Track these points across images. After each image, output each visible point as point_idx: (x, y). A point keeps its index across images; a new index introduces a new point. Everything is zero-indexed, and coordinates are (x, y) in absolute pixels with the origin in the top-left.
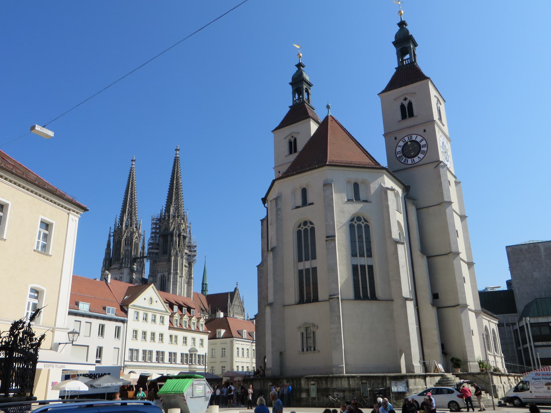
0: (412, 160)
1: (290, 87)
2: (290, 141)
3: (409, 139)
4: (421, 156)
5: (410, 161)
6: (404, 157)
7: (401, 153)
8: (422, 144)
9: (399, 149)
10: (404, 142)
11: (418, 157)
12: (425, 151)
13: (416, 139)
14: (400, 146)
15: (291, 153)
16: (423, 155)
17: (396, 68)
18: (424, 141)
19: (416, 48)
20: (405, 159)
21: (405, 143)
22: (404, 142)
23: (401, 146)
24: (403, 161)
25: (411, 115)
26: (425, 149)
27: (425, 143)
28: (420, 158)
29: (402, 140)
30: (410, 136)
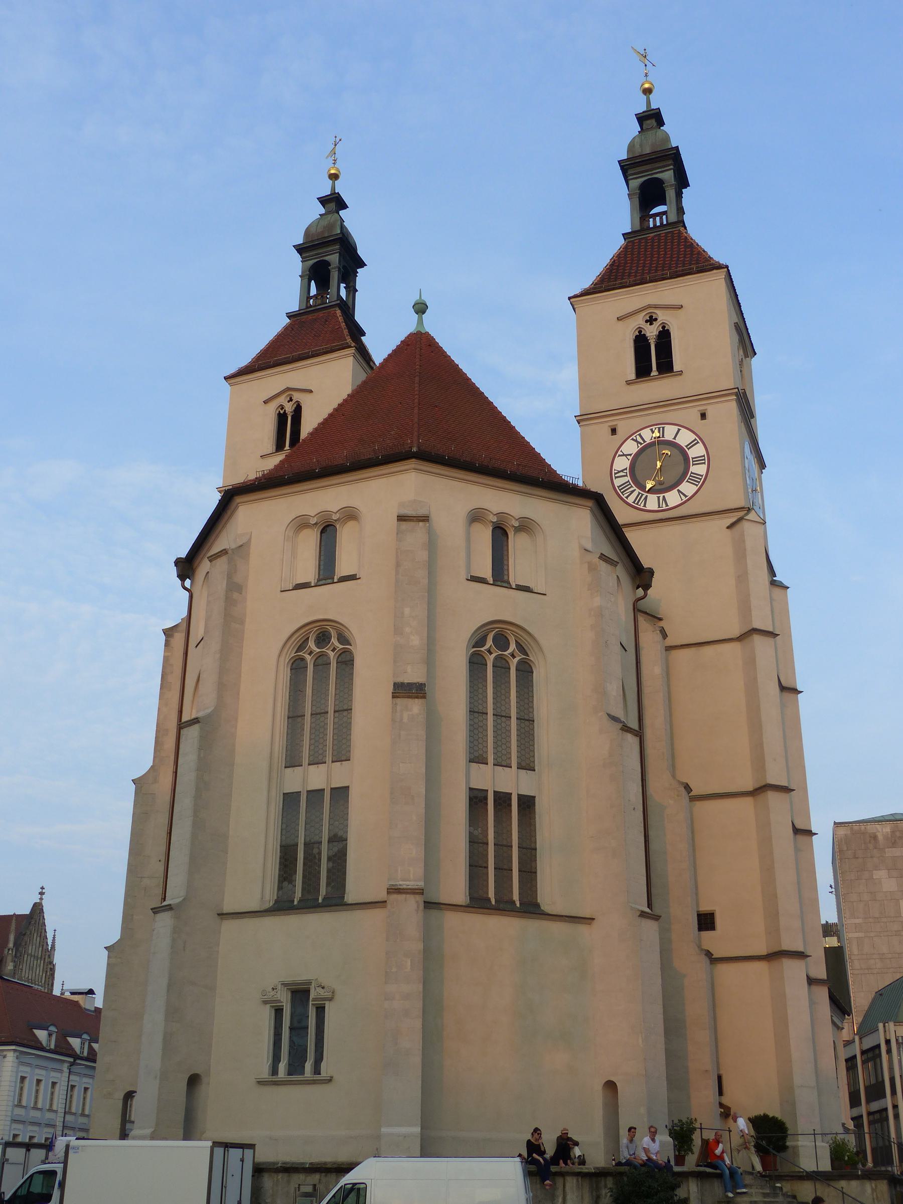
0: (659, 498)
1: (297, 257)
2: (282, 412)
4: (688, 488)
5: (652, 502)
7: (626, 476)
8: (692, 453)
9: (622, 463)
10: (638, 442)
11: (679, 491)
12: (695, 439)
13: (675, 438)
14: (626, 455)
16: (695, 488)
17: (290, 316)
21: (640, 446)
22: (638, 442)
23: (630, 455)
24: (631, 500)
25: (666, 367)
26: (701, 469)
27: (704, 452)
29: (633, 437)
30: (659, 428)
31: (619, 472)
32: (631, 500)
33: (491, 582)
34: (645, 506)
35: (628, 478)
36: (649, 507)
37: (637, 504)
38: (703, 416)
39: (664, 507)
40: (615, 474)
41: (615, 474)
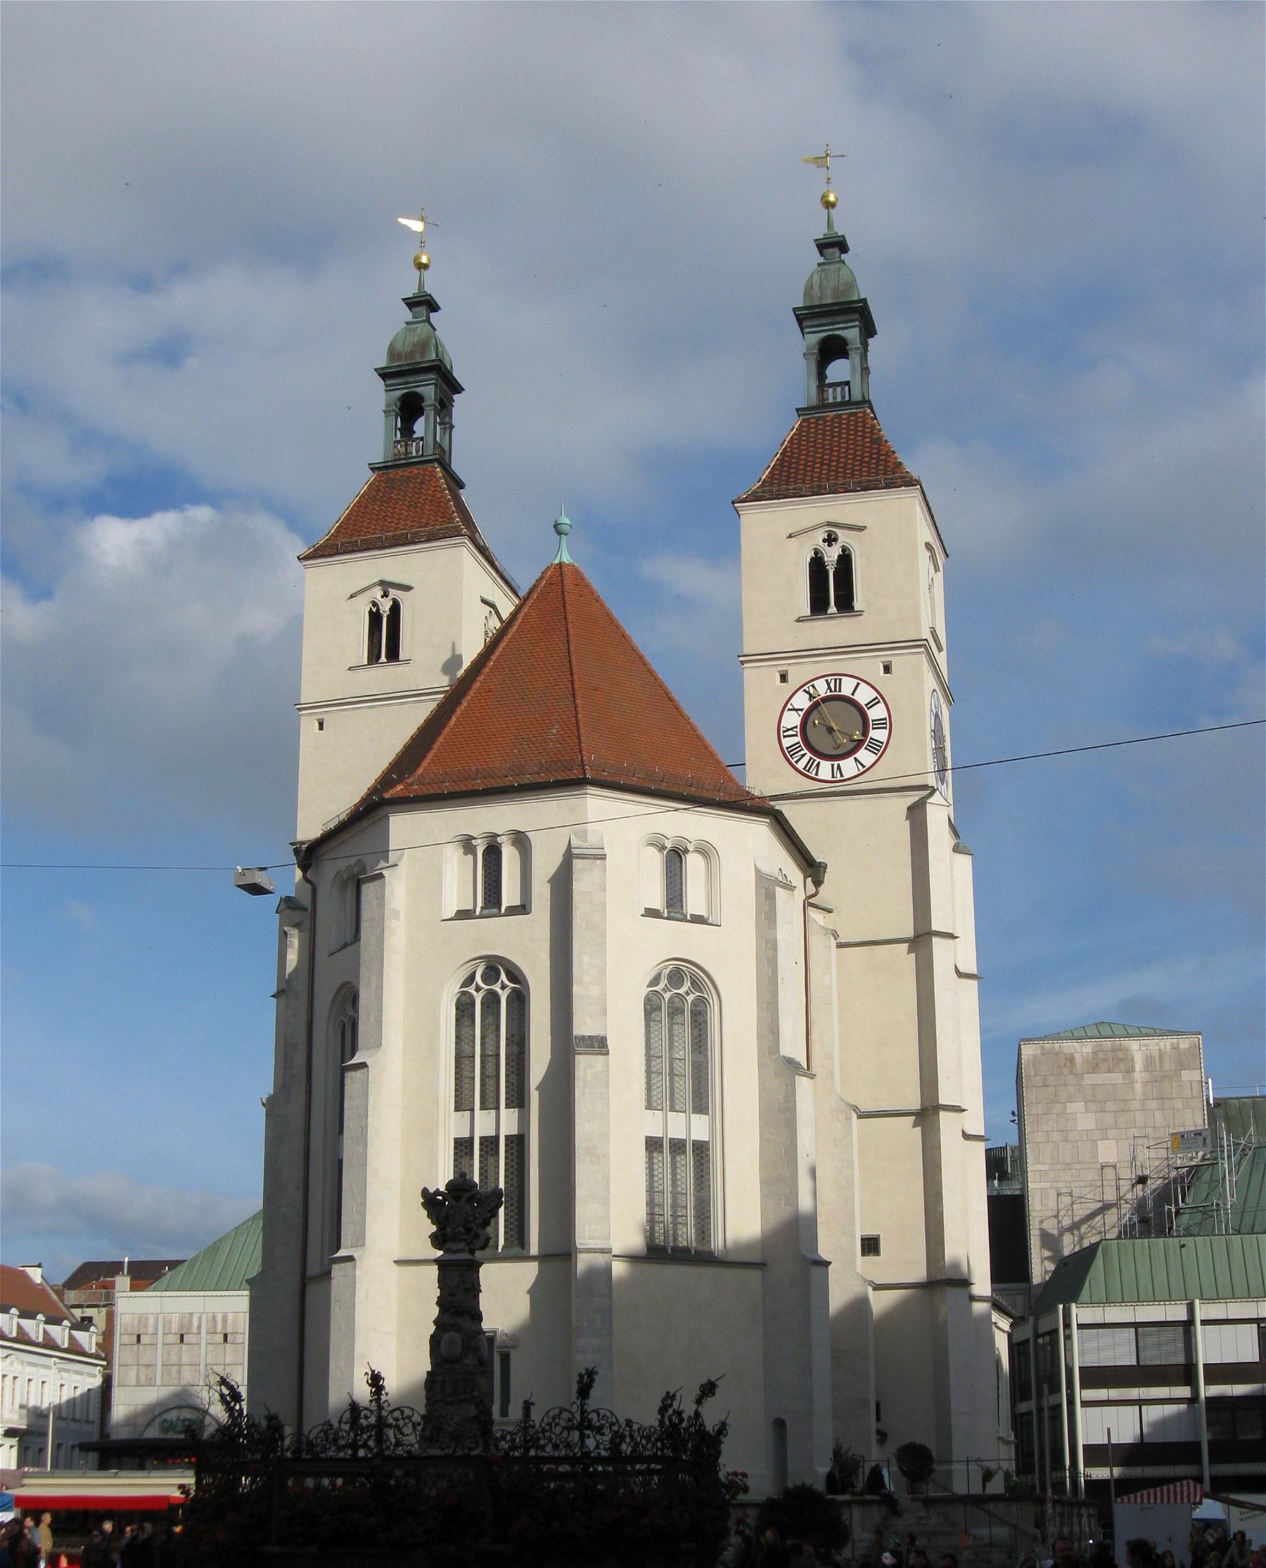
3: (829, 688)
4: (865, 756)
5: (825, 768)
6: (805, 751)
7: (796, 735)
9: (792, 720)
11: (856, 759)
13: (853, 694)
14: (796, 710)
15: (374, 658)
16: (875, 758)
18: (882, 705)
19: (456, 397)
20: (811, 758)
23: (801, 710)
24: (801, 765)
25: (846, 603)
27: (885, 715)
28: (864, 766)
30: (836, 680)
31: (788, 730)
32: (801, 765)
33: (666, 915)
34: (817, 774)
35: (798, 739)
36: (820, 777)
37: (808, 771)
38: (887, 669)
39: (839, 778)
40: (784, 732)
41: (784, 732)
